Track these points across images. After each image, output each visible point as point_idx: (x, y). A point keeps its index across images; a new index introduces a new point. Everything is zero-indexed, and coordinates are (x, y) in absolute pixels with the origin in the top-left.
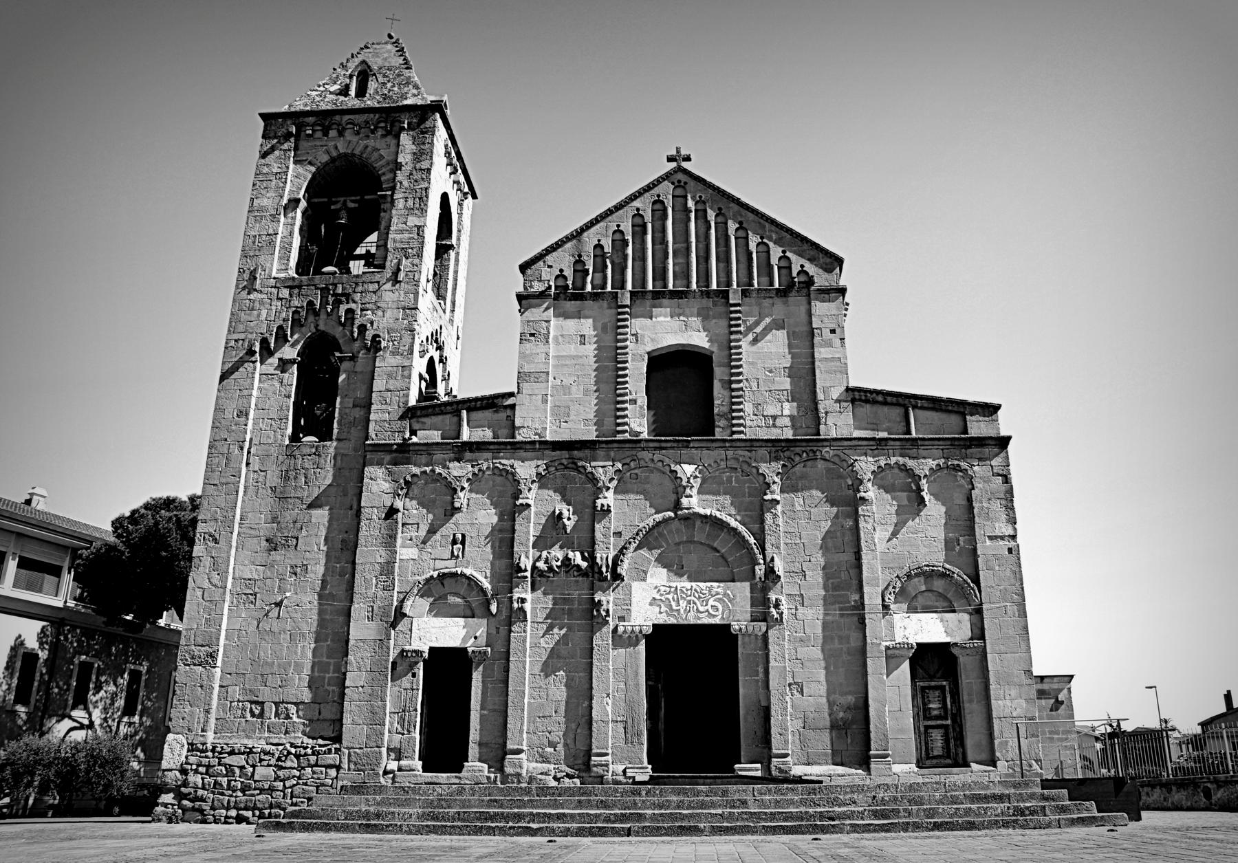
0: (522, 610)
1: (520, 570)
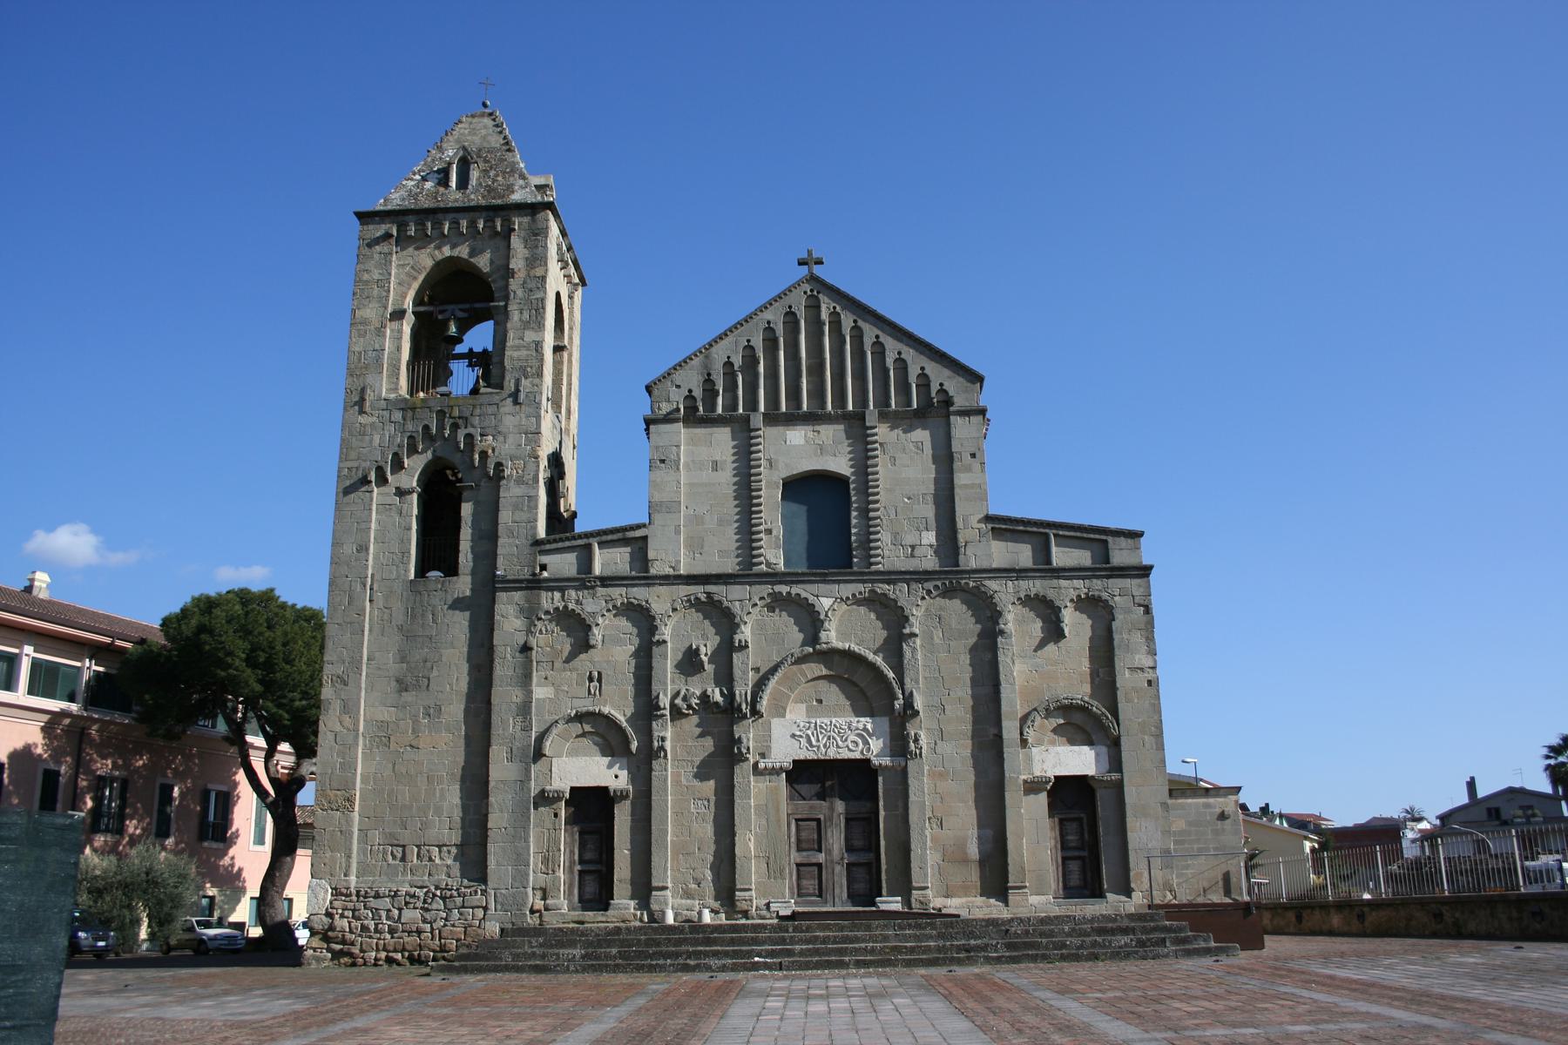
0: (662, 748)
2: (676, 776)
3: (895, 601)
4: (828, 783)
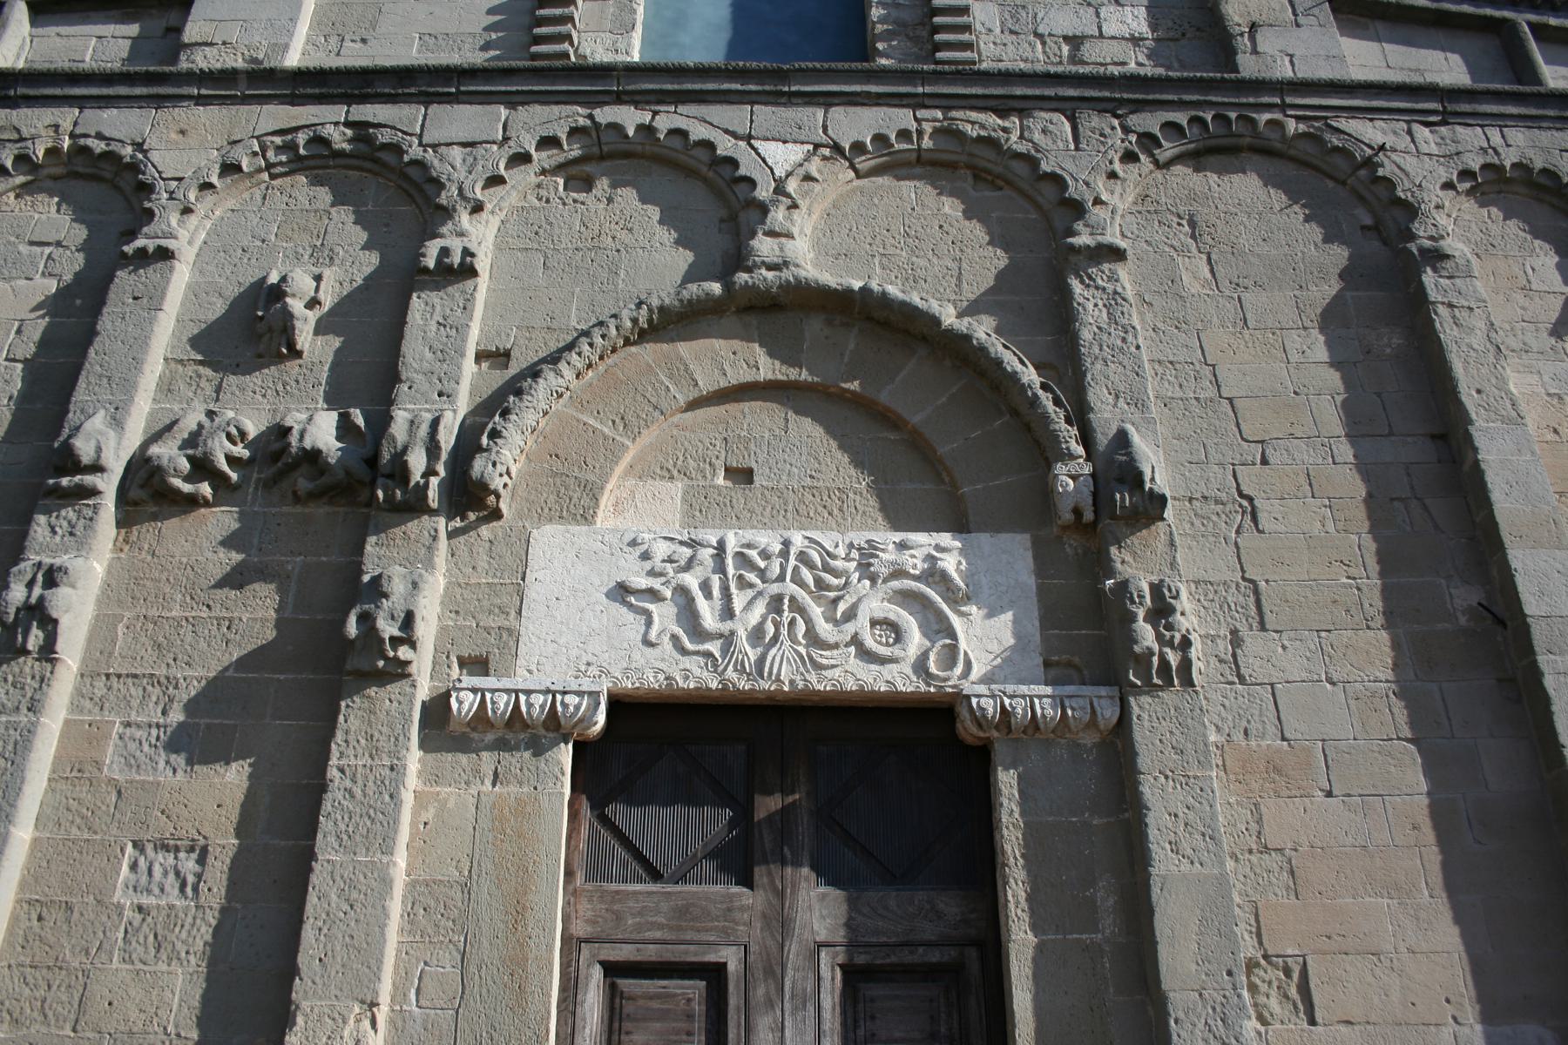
0: (38, 613)
1: (69, 462)
2: (82, 741)
3: (1031, 161)
4: (768, 805)
